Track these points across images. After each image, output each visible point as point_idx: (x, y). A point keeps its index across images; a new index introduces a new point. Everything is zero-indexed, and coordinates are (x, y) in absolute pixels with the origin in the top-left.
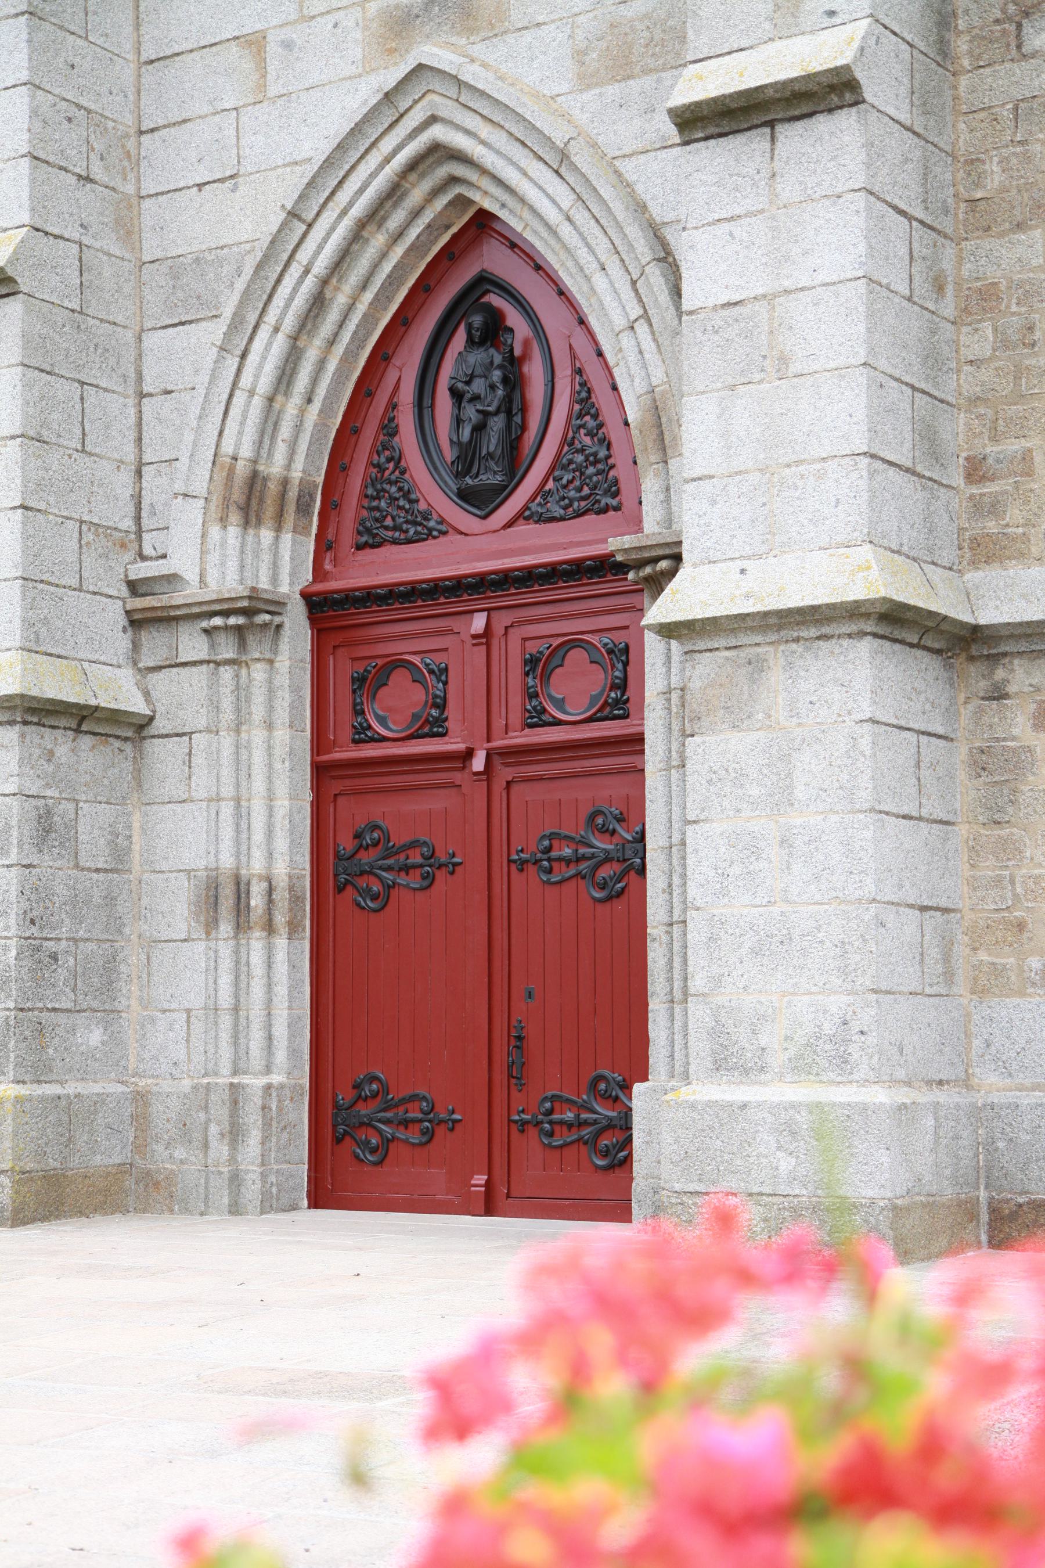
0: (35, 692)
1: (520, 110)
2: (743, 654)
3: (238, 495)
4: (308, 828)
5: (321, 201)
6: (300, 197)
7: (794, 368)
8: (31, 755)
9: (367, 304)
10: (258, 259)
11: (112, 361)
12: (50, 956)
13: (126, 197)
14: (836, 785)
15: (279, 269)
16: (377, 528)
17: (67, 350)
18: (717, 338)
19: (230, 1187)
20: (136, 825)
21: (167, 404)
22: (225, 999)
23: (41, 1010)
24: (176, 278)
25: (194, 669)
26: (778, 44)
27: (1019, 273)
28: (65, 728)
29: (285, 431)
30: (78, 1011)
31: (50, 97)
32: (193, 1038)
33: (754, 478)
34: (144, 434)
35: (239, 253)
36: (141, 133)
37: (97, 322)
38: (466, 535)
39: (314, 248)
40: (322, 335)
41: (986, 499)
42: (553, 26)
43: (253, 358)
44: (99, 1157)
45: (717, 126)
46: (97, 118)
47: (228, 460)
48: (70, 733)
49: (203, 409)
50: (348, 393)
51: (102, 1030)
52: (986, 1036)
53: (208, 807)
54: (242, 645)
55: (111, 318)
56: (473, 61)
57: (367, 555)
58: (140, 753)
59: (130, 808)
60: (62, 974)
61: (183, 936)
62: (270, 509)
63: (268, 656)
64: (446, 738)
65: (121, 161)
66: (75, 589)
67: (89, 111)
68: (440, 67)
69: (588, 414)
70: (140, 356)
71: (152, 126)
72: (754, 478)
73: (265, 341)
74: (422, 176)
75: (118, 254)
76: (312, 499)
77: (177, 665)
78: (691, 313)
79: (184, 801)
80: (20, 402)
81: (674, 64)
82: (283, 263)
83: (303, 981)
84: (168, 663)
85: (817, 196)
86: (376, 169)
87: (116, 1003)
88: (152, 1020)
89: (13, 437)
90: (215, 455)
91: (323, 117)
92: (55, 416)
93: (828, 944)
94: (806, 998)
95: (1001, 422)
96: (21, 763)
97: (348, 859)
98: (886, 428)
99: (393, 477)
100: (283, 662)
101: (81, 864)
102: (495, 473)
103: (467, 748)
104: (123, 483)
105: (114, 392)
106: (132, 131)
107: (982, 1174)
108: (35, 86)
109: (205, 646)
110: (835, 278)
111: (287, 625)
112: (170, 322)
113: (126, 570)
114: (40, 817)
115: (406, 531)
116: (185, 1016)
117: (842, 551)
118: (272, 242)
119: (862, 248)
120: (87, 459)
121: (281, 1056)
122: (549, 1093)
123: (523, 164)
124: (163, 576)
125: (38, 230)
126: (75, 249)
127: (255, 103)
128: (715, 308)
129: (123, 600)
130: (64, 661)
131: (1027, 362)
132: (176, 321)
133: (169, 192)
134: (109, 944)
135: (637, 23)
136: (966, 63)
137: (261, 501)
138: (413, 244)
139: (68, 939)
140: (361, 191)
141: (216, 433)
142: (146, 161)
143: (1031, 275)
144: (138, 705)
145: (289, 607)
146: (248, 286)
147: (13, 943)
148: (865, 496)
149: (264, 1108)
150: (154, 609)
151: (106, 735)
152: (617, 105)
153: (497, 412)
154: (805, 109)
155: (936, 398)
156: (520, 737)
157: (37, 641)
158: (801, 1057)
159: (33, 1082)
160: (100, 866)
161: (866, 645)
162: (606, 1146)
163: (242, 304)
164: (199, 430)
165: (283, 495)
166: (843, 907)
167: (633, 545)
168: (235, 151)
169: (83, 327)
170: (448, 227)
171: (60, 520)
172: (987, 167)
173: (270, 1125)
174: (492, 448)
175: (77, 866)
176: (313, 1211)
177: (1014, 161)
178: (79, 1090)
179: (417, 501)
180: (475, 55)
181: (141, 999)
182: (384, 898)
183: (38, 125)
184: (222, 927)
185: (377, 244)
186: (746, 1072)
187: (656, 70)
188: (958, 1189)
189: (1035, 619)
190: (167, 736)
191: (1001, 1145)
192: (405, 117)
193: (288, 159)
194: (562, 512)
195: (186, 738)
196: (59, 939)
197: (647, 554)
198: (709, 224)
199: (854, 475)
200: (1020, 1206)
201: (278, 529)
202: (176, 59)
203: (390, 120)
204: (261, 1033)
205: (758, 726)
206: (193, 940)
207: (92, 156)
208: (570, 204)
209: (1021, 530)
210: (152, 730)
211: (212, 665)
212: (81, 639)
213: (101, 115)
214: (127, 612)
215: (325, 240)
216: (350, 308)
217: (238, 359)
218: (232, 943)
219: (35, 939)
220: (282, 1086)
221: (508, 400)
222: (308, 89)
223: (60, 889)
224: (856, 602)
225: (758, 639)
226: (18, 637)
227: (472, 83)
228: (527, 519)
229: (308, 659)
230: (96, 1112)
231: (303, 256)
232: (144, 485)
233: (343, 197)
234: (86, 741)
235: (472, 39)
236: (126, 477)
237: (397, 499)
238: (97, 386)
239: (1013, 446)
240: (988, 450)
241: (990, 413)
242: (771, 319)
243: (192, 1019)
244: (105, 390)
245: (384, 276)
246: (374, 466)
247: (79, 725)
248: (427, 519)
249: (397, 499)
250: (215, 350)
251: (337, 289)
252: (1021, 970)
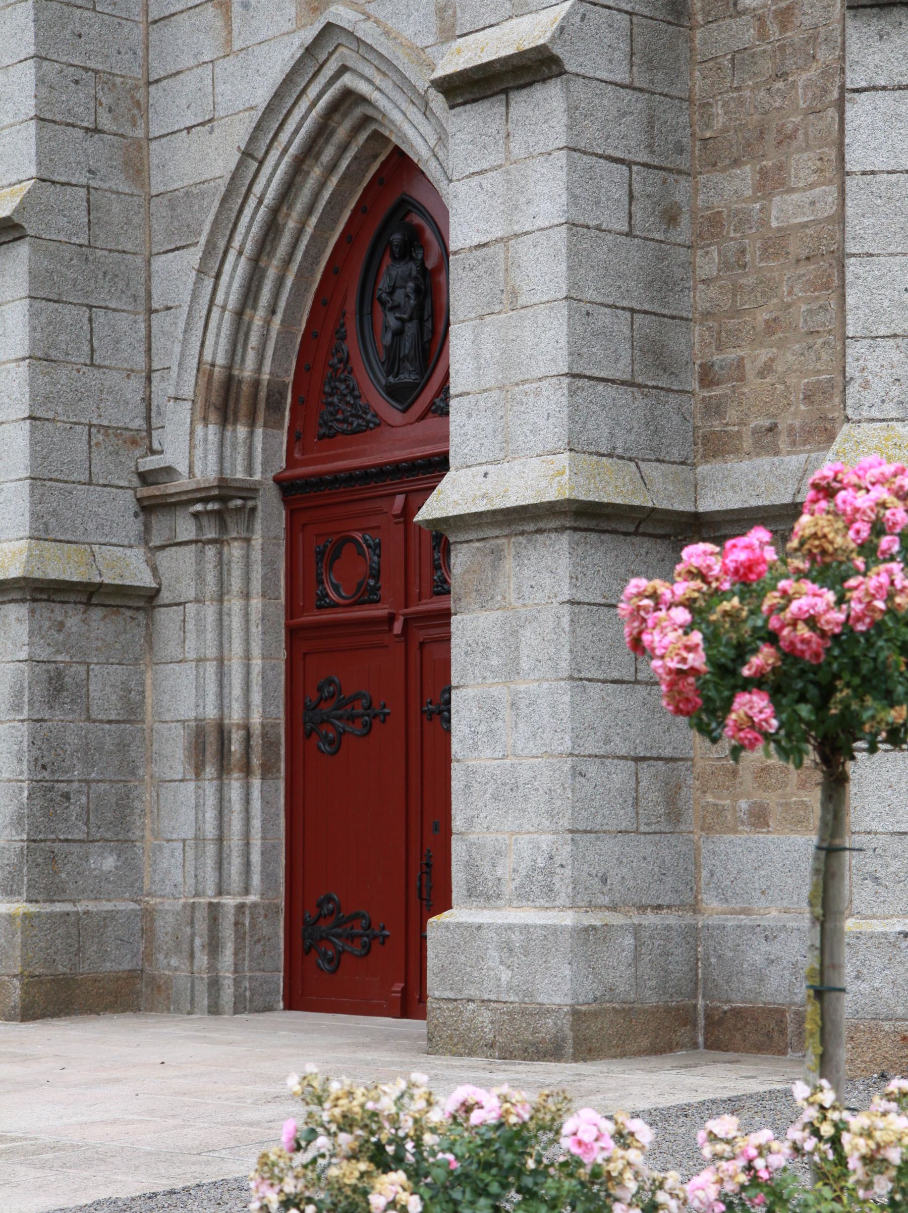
0: (37, 575)
1: (395, 62)
2: (489, 544)
3: (214, 398)
4: (283, 683)
5: (268, 141)
6: (250, 139)
7: (523, 300)
8: (40, 627)
11: (121, 285)
12: (62, 796)
13: (136, 142)
14: (547, 657)
15: (240, 201)
17: (75, 280)
18: (471, 274)
19: (209, 991)
20: (148, 682)
22: (210, 830)
23: (54, 841)
24: (173, 209)
25: (187, 548)
26: (514, 21)
27: (736, 203)
28: (75, 603)
29: (254, 340)
30: (92, 841)
31: (57, 65)
32: (187, 864)
33: (495, 394)
36: (149, 83)
37: (106, 253)
41: (713, 401)
43: (225, 278)
44: (108, 964)
45: (470, 93)
46: (104, 77)
47: (208, 367)
48: (79, 606)
50: (310, 303)
51: (115, 857)
52: (711, 867)
53: (197, 666)
54: (223, 527)
55: (120, 247)
56: (368, 18)
58: (150, 618)
59: (143, 667)
60: (74, 810)
61: (180, 777)
62: (243, 409)
63: (244, 535)
65: (130, 110)
66: (84, 484)
67: (96, 72)
68: (341, 25)
70: (149, 278)
71: (156, 77)
72: (495, 394)
74: (345, 115)
75: (127, 191)
76: (283, 397)
78: (455, 253)
80: (28, 329)
83: (278, 815)
85: (535, 154)
87: (130, 834)
88: (160, 848)
89: (24, 359)
91: (270, 68)
92: (62, 337)
93: (541, 791)
94: (526, 837)
95: (723, 334)
96: (31, 634)
97: (314, 709)
98: (594, 350)
99: (343, 376)
100: (257, 541)
101: (93, 717)
102: (410, 372)
103: (390, 614)
104: (133, 389)
105: (123, 311)
106: (141, 83)
107: (700, 985)
108: (41, 58)
110: (547, 224)
111: (260, 508)
114: (51, 678)
115: (352, 424)
117: (550, 457)
118: (232, 178)
119: (564, 199)
120: (96, 372)
121: (256, 880)
125: (44, 181)
126: (82, 192)
128: (470, 249)
129: (134, 489)
130: (74, 546)
131: (741, 281)
132: (173, 246)
134: (121, 784)
136: (700, 18)
137: (237, 400)
138: (344, 174)
139: (80, 781)
140: (296, 131)
141: (199, 344)
143: (744, 205)
144: (146, 580)
145: (261, 493)
147: (25, 785)
148: (566, 410)
149: (236, 924)
150: (155, 497)
151: (117, 606)
153: (410, 319)
154: (527, 79)
155: (664, 316)
157: (46, 530)
158: (522, 886)
159: (45, 901)
160: (113, 717)
161: (564, 541)
163: (212, 233)
164: (185, 342)
165: (255, 395)
166: (551, 760)
168: (211, 98)
169: (91, 258)
170: (375, 157)
171: (68, 426)
172: (714, 110)
173: (244, 939)
174: (407, 351)
175: (89, 719)
177: (733, 105)
178: (90, 908)
179: (360, 397)
180: (371, 12)
181: (152, 830)
182: (336, 744)
183: (44, 91)
184: (208, 770)
186: (488, 898)
188: (666, 998)
189: (736, 507)
191: (713, 960)
193: (247, 105)
195: (181, 607)
196: (71, 781)
198: (467, 177)
199: (559, 393)
200: (725, 1012)
201: (252, 425)
202: (173, 19)
204: (239, 860)
205: (497, 606)
207: (100, 110)
209: (736, 428)
211: (200, 544)
212: (91, 526)
213: (110, 74)
214: (139, 500)
215: (272, 174)
216: (300, 232)
218: (215, 782)
219: (47, 781)
220: (254, 905)
221: (420, 307)
223: (72, 740)
224: (550, 502)
225: (497, 532)
226: (27, 528)
229: (283, 535)
230: (105, 926)
231: (257, 189)
233: (284, 137)
234: (96, 614)
236: (136, 383)
238: (106, 308)
239: (731, 355)
240: (715, 358)
241: (716, 325)
242: (506, 258)
244: (115, 310)
245: (324, 203)
247: (89, 599)
248: (366, 413)
250: (194, 272)
251: (288, 215)
252: (734, 808)
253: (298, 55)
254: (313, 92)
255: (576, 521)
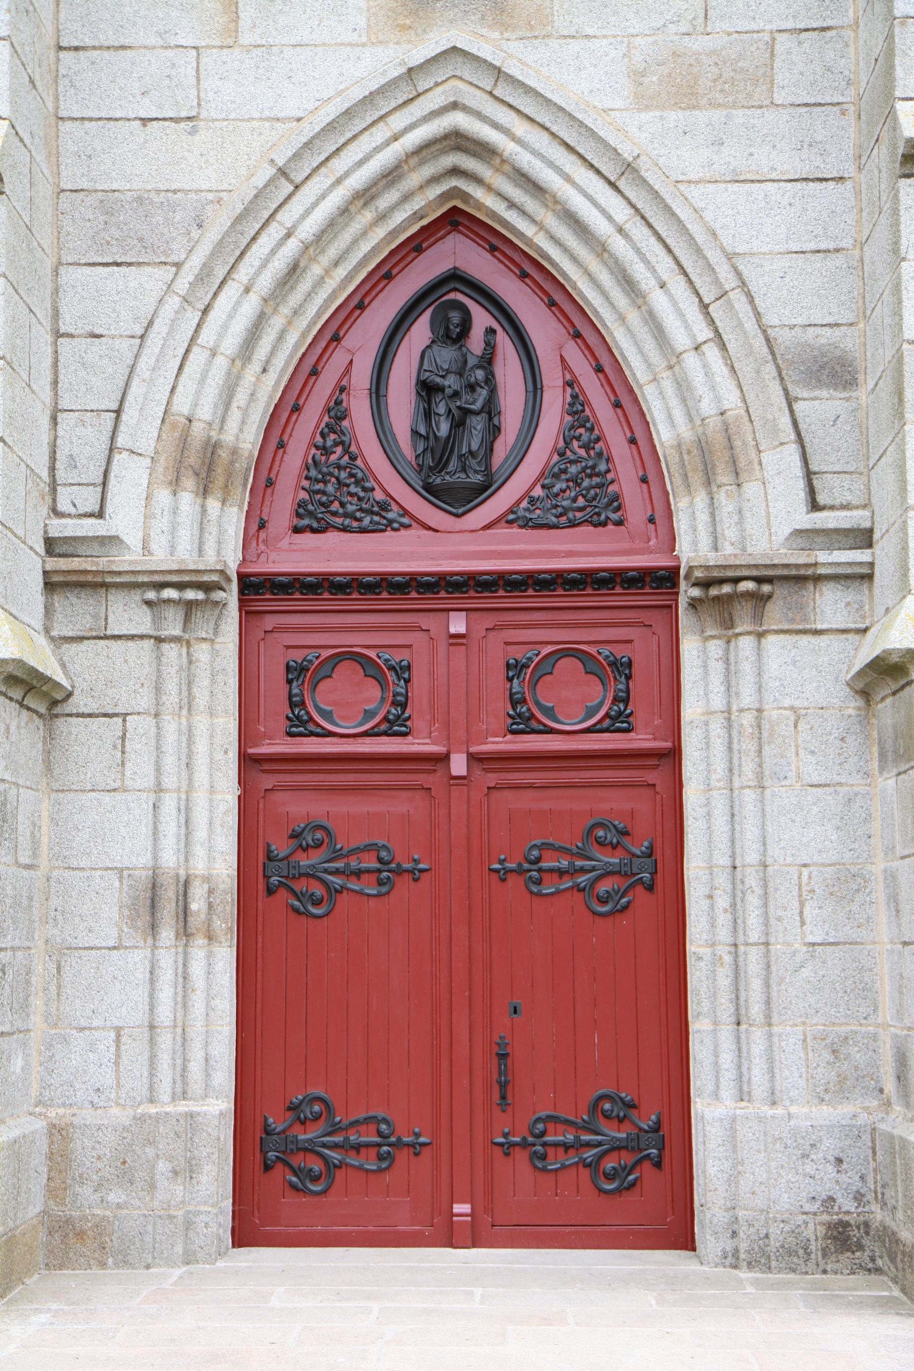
3: (193, 459)
5: (315, 165)
6: (294, 155)
9: (338, 280)
10: (239, 211)
15: (258, 226)
16: (322, 513)
21: (94, 349)
22: (165, 1014)
25: (130, 644)
34: (61, 377)
35: (198, 201)
36: (60, 48)
38: (437, 531)
39: (301, 212)
40: (291, 303)
42: (605, 41)
49: (158, 360)
57: (308, 539)
61: (111, 943)
63: (211, 636)
64: (410, 738)
69: (584, 426)
70: (56, 291)
73: (234, 300)
77: (106, 637)
79: (115, 790)
81: (746, 104)
82: (263, 221)
84: (94, 634)
86: (382, 144)
88: (65, 1040)
90: (165, 412)
109: (149, 619)
112: (100, 260)
113: (46, 525)
115: (360, 520)
116: (113, 1035)
118: (256, 196)
122: (543, 1114)
123: (568, 169)
124: (98, 537)
127: (222, 47)
133: (100, 119)
135: (703, 57)
140: (361, 163)
141: (169, 389)
142: (66, 81)
146: (223, 238)
152: (681, 131)
156: (501, 743)
162: (614, 1168)
167: (719, 563)
174: (475, 446)
176: (235, 1250)
179: (373, 489)
181: (47, 1015)
185: (364, 220)
187: (725, 106)
190: (90, 715)
192: (422, 98)
193: (267, 113)
194: (554, 519)
195: (119, 720)
197: (730, 574)
203: (405, 97)
206: (126, 948)
208: (626, 218)
210: (69, 708)
214: (45, 573)
217: (200, 314)
222: (294, 46)
227: (520, 78)
228: (510, 522)
231: (287, 217)
232: (60, 432)
233: (340, 165)
235: (506, 35)
237: (348, 486)
243: (123, 1039)
246: (317, 448)
249: (348, 486)
253: (395, 74)
254: (398, 121)
255: (896, 679)
